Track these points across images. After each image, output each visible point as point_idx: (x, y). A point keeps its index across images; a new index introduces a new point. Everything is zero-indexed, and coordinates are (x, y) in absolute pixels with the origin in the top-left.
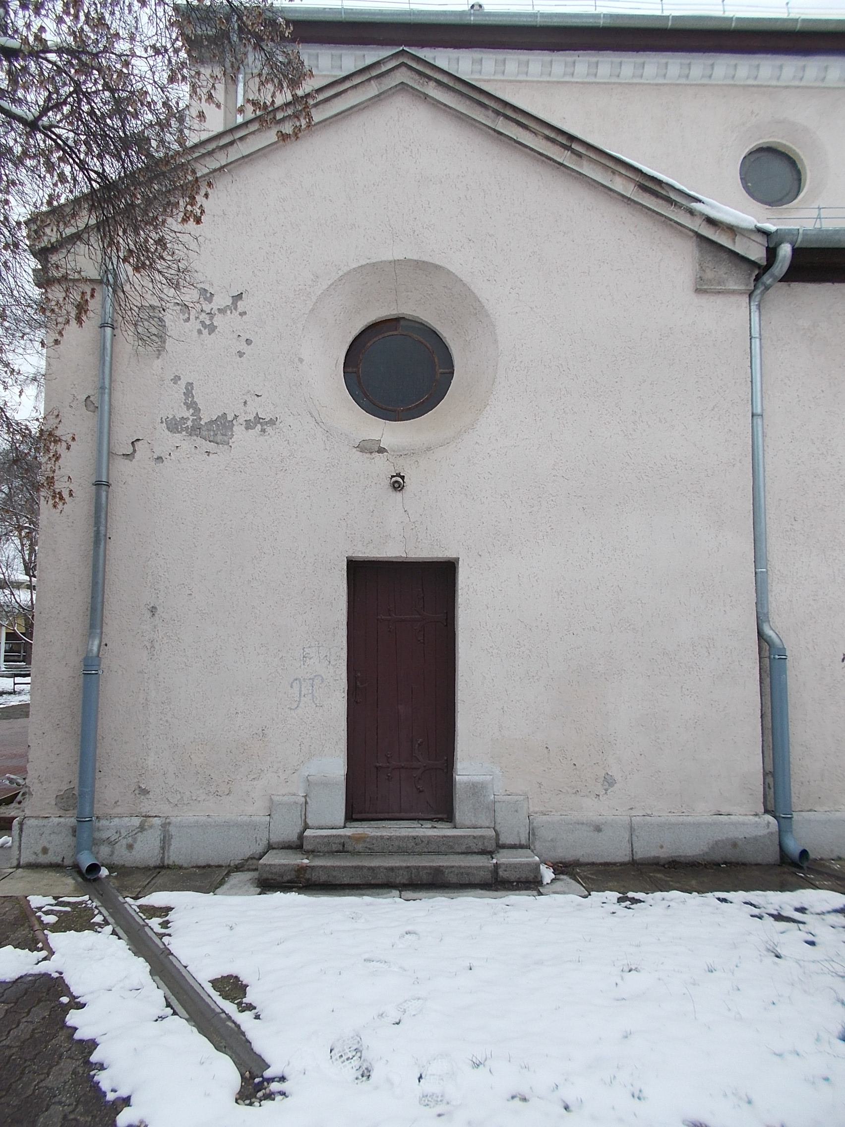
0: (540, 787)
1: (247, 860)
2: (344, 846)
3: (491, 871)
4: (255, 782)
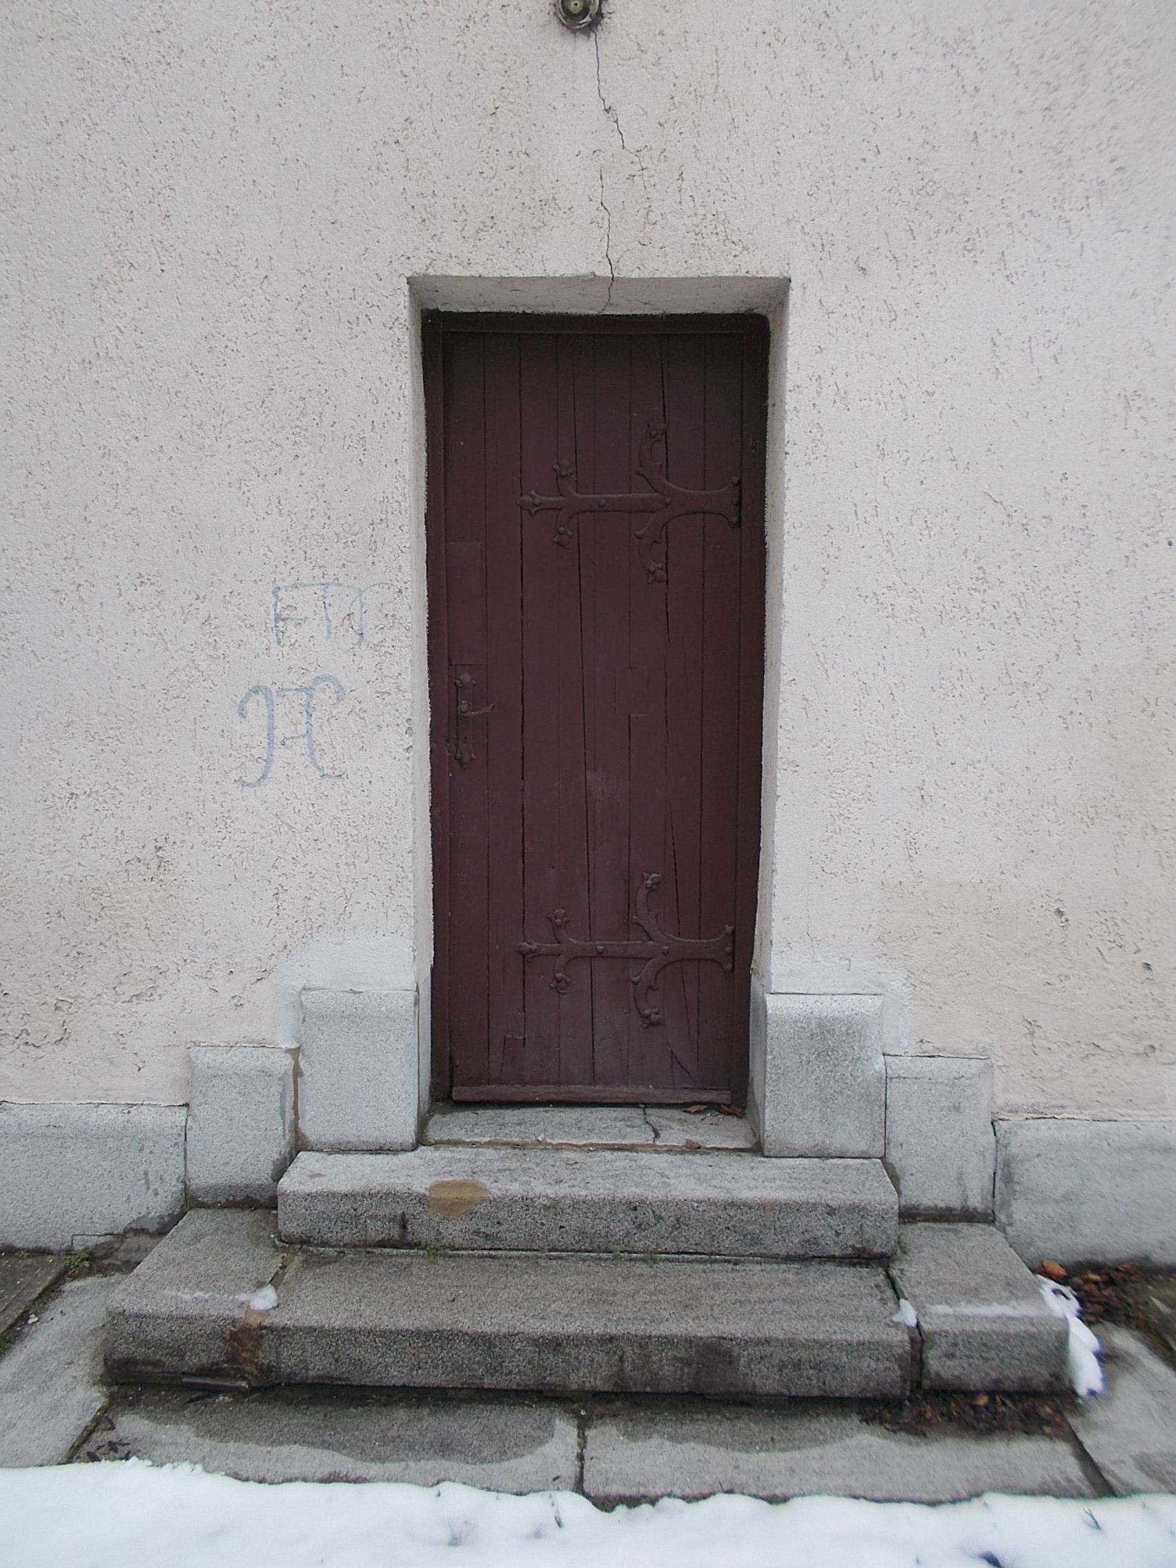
0: (1032, 1033)
1: (122, 1237)
2: (404, 1226)
3: (900, 1359)
4: (141, 1008)
